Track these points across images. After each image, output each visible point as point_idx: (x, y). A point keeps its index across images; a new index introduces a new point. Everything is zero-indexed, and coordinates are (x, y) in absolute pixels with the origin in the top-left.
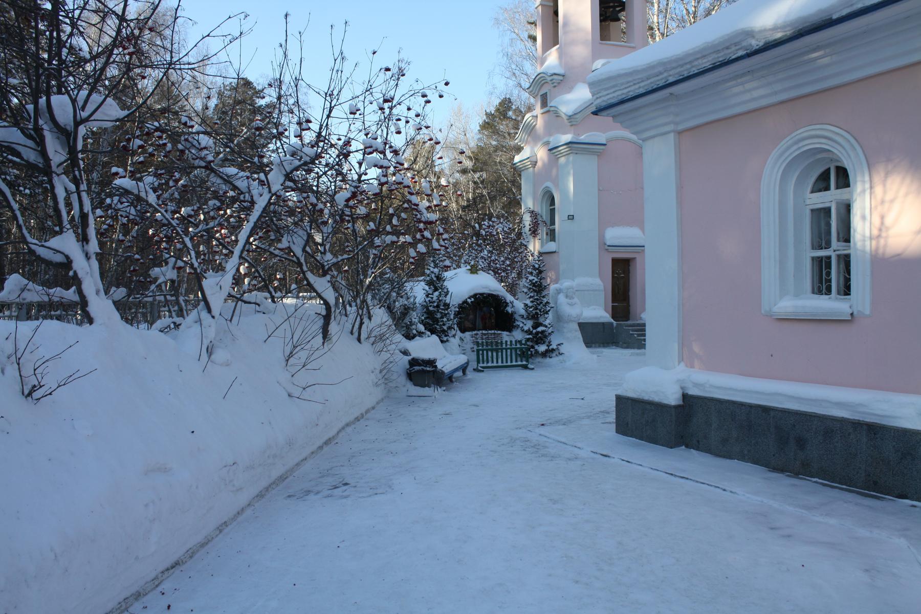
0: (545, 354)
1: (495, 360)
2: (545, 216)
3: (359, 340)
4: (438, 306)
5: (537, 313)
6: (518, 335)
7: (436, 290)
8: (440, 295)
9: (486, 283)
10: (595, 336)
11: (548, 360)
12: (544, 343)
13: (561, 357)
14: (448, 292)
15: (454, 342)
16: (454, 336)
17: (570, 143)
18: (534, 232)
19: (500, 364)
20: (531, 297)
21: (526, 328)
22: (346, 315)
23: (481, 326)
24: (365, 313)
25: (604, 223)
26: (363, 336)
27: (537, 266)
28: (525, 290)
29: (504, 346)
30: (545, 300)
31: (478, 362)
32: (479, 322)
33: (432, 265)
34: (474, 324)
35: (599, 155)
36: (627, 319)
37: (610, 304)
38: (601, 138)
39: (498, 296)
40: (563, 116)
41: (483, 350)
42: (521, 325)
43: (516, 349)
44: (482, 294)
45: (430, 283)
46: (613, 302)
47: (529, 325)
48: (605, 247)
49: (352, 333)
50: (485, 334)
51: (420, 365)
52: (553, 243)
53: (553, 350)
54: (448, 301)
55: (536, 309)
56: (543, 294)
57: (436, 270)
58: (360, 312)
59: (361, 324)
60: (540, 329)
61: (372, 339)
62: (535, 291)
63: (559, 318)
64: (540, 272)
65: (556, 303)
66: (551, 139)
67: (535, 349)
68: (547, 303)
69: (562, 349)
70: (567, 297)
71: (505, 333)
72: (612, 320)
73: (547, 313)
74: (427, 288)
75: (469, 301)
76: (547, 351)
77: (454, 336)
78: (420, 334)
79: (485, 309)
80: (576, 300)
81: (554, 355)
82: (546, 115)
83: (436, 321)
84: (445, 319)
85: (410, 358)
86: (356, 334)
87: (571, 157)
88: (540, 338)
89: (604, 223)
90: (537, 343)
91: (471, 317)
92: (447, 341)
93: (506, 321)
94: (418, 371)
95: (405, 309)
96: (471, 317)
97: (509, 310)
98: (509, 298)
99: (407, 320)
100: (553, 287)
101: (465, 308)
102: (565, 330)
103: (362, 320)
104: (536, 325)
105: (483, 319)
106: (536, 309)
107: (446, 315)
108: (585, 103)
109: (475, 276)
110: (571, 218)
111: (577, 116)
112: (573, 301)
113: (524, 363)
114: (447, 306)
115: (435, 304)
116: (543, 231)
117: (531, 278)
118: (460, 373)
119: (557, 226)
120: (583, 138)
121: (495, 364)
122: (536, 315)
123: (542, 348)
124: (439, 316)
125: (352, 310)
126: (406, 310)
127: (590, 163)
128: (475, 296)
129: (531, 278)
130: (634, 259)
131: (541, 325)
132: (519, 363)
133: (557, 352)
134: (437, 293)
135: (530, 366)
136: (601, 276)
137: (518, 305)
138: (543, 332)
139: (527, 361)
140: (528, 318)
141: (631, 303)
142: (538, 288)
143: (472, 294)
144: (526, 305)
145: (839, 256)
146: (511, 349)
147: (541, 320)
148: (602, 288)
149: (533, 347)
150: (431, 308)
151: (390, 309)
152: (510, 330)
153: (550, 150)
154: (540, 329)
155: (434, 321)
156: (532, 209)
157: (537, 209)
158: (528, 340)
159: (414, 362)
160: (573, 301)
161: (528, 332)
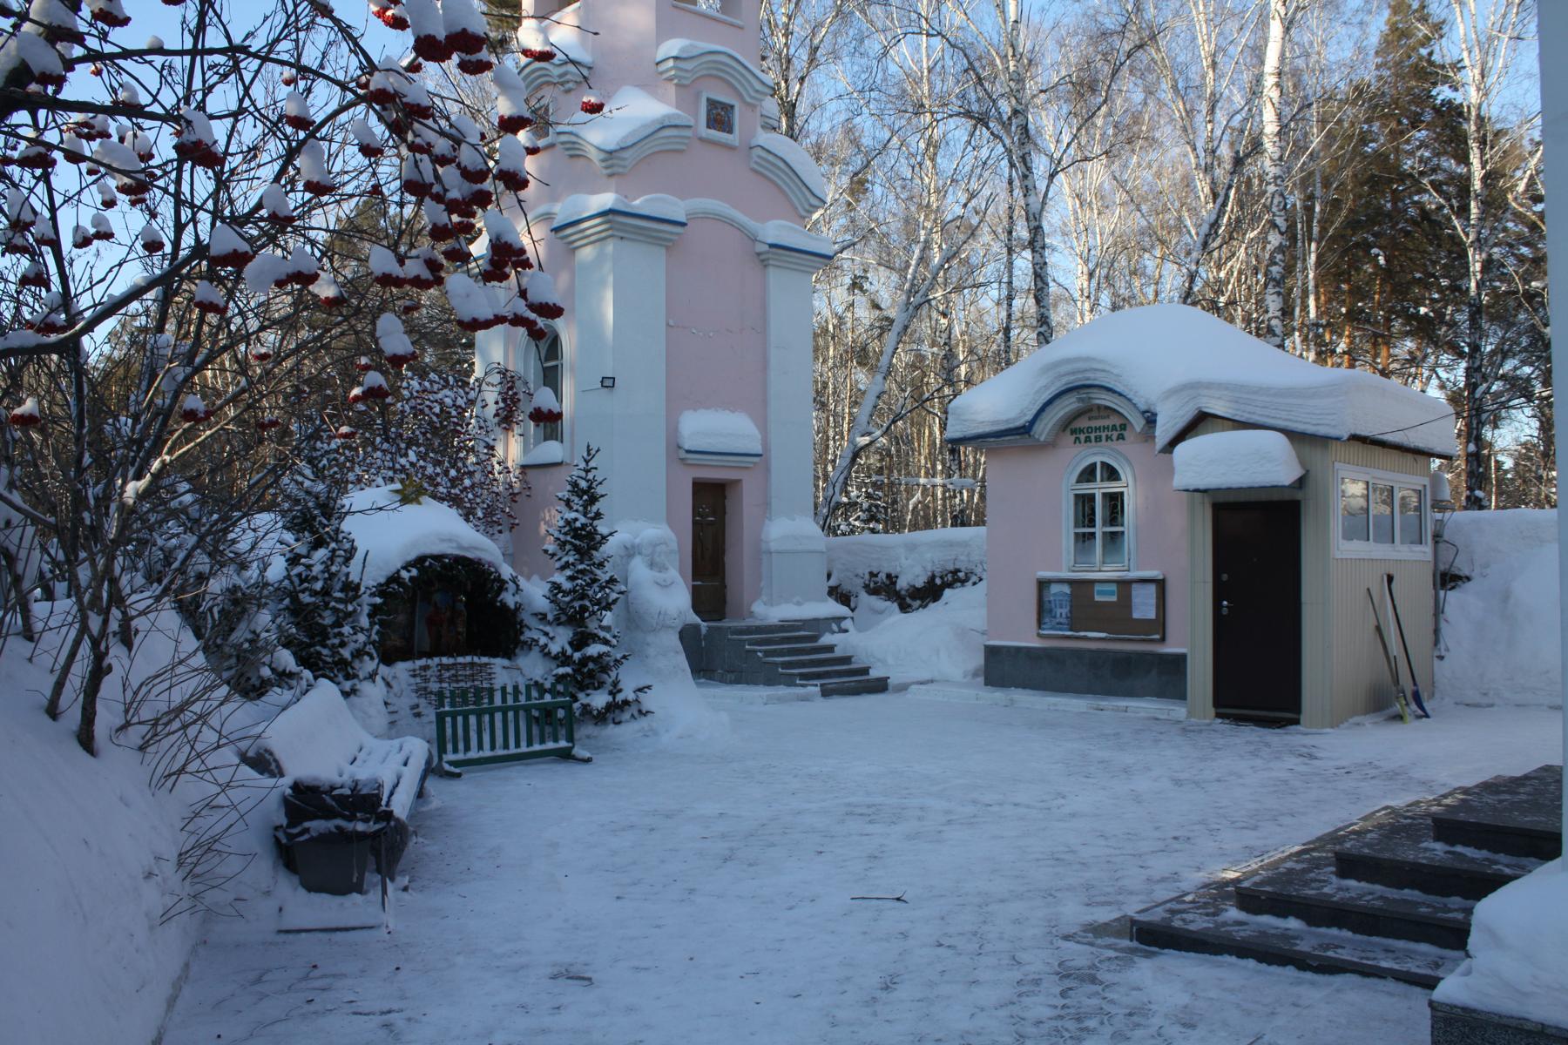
3: (86, 739)
4: (325, 592)
5: (583, 609)
6: (533, 667)
7: (318, 544)
8: (332, 559)
9: (434, 527)
11: (611, 730)
12: (601, 685)
13: (643, 722)
14: (353, 550)
15: (373, 692)
16: (372, 677)
17: (611, 212)
18: (506, 419)
20: (566, 566)
21: (555, 648)
22: (28, 634)
24: (106, 629)
25: (679, 398)
26: (106, 718)
27: (583, 484)
28: (551, 548)
29: (498, 701)
30: (603, 577)
35: (668, 245)
38: (675, 208)
40: (594, 155)
41: (454, 716)
42: (543, 640)
43: (527, 709)
44: (438, 558)
45: (301, 523)
47: (561, 639)
48: (679, 454)
49: (53, 711)
50: (447, 667)
51: (329, 814)
53: (626, 703)
54: (354, 578)
55: (583, 596)
56: (597, 556)
58: (95, 623)
59: (99, 671)
60: (594, 649)
61: (135, 734)
63: (635, 620)
64: (593, 499)
66: (557, 208)
69: (648, 701)
70: (652, 565)
71: (499, 662)
72: (698, 620)
74: (289, 537)
75: (404, 574)
76: (610, 707)
78: (284, 677)
81: (626, 716)
83: (321, 634)
84: (346, 630)
85: (285, 783)
86: (73, 716)
87: (610, 247)
89: (679, 398)
94: (324, 838)
95: (236, 602)
97: (509, 599)
99: (240, 635)
101: (394, 595)
102: (651, 651)
103: (99, 656)
104: (580, 641)
107: (349, 614)
108: (644, 126)
110: (608, 383)
111: (625, 154)
113: (563, 744)
114: (351, 589)
115: (318, 586)
120: (639, 204)
121: (487, 753)
123: (599, 700)
124: (328, 619)
125: (55, 614)
126: (239, 604)
127: (649, 264)
128: (419, 561)
130: (738, 482)
131: (595, 638)
132: (550, 745)
133: (634, 710)
134: (321, 553)
135: (579, 751)
137: (533, 592)
139: (570, 739)
140: (558, 622)
141: (729, 580)
143: (412, 556)
144: (556, 587)
145: (1104, 495)
146: (516, 710)
147: (592, 626)
148: (674, 546)
150: (306, 598)
151: (190, 612)
152: (509, 654)
153: (556, 230)
154: (594, 649)
155: (317, 632)
157: (516, 366)
158: (560, 679)
159: (307, 800)
161: (563, 659)
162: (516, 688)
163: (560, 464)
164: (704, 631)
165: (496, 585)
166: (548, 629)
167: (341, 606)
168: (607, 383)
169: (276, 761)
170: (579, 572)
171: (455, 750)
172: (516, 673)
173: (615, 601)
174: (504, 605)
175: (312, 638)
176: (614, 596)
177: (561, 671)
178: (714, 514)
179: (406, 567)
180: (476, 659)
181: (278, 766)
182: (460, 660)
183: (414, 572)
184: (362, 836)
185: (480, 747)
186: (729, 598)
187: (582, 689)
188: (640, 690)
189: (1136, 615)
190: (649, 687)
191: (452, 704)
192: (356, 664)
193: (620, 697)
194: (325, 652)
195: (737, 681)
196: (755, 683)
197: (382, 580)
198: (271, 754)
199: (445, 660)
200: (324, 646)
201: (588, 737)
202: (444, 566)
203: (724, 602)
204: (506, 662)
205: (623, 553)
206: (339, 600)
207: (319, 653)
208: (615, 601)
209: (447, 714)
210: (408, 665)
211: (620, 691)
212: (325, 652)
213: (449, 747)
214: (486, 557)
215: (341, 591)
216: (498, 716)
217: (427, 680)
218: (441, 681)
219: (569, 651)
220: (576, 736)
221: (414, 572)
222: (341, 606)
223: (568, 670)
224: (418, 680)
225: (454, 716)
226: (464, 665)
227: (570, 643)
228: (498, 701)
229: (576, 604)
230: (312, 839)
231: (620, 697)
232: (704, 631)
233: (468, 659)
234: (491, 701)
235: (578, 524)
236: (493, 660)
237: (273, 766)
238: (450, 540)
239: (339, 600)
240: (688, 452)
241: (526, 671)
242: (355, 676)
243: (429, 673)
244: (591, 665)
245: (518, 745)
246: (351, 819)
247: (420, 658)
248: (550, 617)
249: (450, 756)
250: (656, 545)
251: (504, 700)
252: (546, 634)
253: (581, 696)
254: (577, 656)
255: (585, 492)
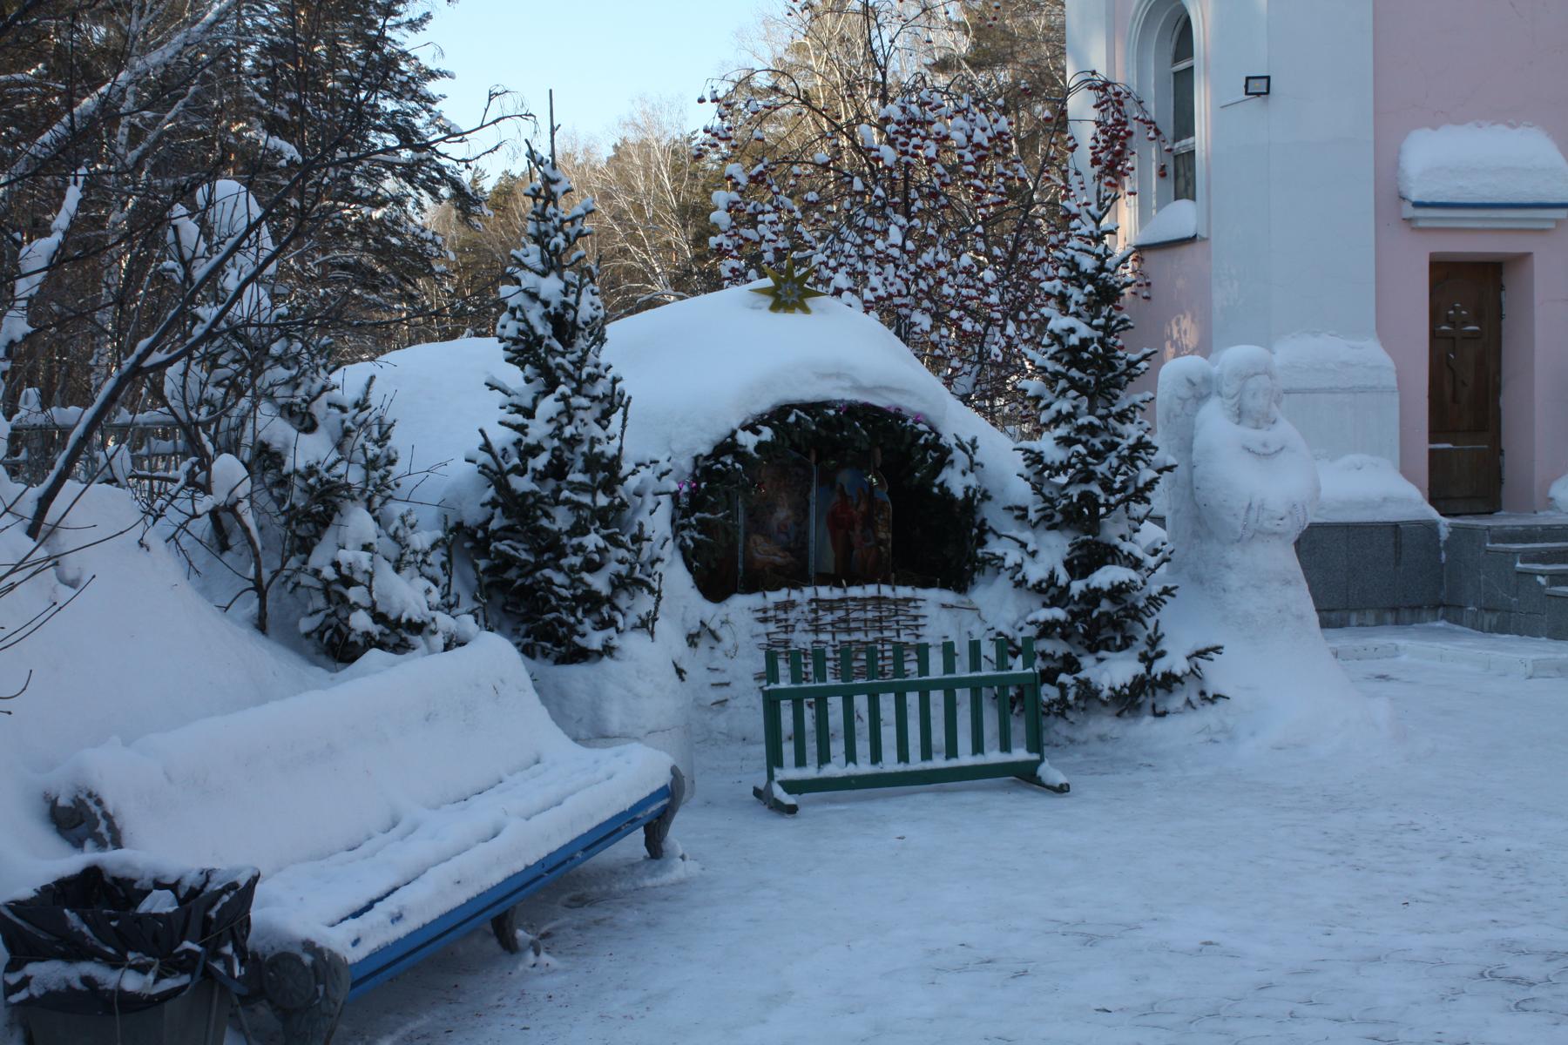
0: (1131, 700)
1: (863, 747)
2: (1157, 104)
4: (557, 469)
5: (1087, 497)
6: (998, 608)
8: (569, 412)
10: (1362, 579)
11: (1146, 726)
12: (1127, 643)
13: (1209, 716)
16: (647, 624)
19: (890, 764)
21: (1035, 572)
23: (829, 566)
27: (1088, 264)
29: (936, 669)
30: (1132, 432)
31: (775, 759)
32: (821, 546)
33: (532, 254)
34: (798, 549)
36: (1491, 504)
37: (1422, 445)
39: (897, 415)
41: (848, 697)
45: (524, 350)
46: (1434, 435)
48: (1401, 210)
50: (831, 606)
52: (1184, 204)
55: (1088, 477)
56: (1123, 404)
57: (551, 287)
60: (1107, 576)
62: (1082, 389)
63: (1202, 520)
65: (1187, 446)
67: (1085, 674)
68: (1142, 445)
69: (1217, 675)
70: (1240, 415)
71: (933, 597)
72: (1434, 514)
73: (1141, 495)
74: (513, 377)
75: (748, 440)
76: (1140, 685)
77: (647, 624)
78: (399, 634)
79: (845, 477)
80: (1285, 430)
81: (1176, 701)
82: (1246, 504)
84: (592, 540)
88: (1107, 621)
90: (1095, 644)
91: (782, 514)
92: (608, 650)
93: (942, 541)
96: (782, 514)
97: (956, 481)
98: (958, 421)
100: (1174, 371)
101: (723, 476)
102: (1233, 580)
104: (1088, 558)
105: (838, 523)
106: (1088, 477)
109: (790, 321)
110: (1259, 87)
112: (1273, 436)
113: (1020, 754)
116: (1145, 159)
117: (1059, 323)
118: (634, 844)
119: (1201, 139)
121: (864, 767)
122: (1083, 513)
123: (1115, 671)
124: (562, 519)
128: (778, 416)
129: (1059, 323)
130: (1523, 258)
131: (1107, 554)
134: (549, 406)
135: (1051, 772)
136: (1384, 333)
137: (994, 456)
138: (1118, 592)
139: (1035, 744)
140: (1047, 521)
142: (1100, 372)
143: (764, 405)
144: (1035, 459)
146: (976, 686)
147: (1112, 531)
148: (1391, 379)
149: (1071, 665)
150: (522, 484)
156: (1102, 73)
157: (1123, 77)
158: (1047, 629)
160: (1273, 436)
161: (1050, 591)
162: (975, 647)
163: (1192, 240)
164: (1444, 533)
165: (932, 455)
166: (1027, 536)
167: (586, 499)
168: (1259, 86)
169: (106, 815)
170: (1080, 429)
171: (800, 762)
172: (968, 616)
173: (1150, 485)
174: (945, 490)
175: (539, 552)
176: (1147, 474)
177: (1045, 614)
178: (1478, 317)
179: (752, 427)
180: (886, 591)
181: (112, 827)
182: (855, 591)
183: (767, 434)
184: (131, 1003)
185: (851, 756)
186: (1507, 474)
187: (1093, 649)
188: (1202, 654)
189: (892, 695)
190: (1217, 649)
191: (796, 676)
192: (623, 601)
193: (1160, 667)
194: (559, 578)
195: (1502, 628)
196: (1533, 632)
197: (705, 450)
198: (99, 802)
199: (824, 592)
200: (559, 569)
201: (1102, 738)
202: (826, 423)
203: (1500, 481)
204: (949, 596)
205: (1185, 392)
206: (579, 488)
207: (550, 581)
208: (1150, 485)
209: (785, 694)
210: (755, 600)
211: (1162, 654)
212: (559, 578)
213: (788, 749)
214: (910, 404)
215: (585, 471)
216: (937, 697)
217: (789, 628)
218: (817, 631)
219: (1063, 577)
220: (1048, 736)
221: (767, 434)
222: (586, 499)
223: (1059, 613)
224: (772, 627)
225: (797, 698)
226: (863, 602)
227: (1068, 565)
228: (936, 669)
229: (1075, 492)
230: (31, 1000)
231: (1160, 667)
232: (1444, 533)
233: (871, 590)
234: (924, 668)
235: (1074, 340)
236: (921, 593)
237: (102, 827)
238: (838, 376)
239: (579, 488)
240: (1417, 205)
241: (989, 612)
242: (612, 623)
243: (793, 615)
244: (1105, 605)
245: (978, 748)
246: (116, 963)
247: (776, 588)
248: (1033, 516)
249: (790, 772)
250: (1246, 377)
251: (949, 666)
252: (1024, 545)
253: (1087, 661)
254: (1077, 587)
255: (1092, 279)
